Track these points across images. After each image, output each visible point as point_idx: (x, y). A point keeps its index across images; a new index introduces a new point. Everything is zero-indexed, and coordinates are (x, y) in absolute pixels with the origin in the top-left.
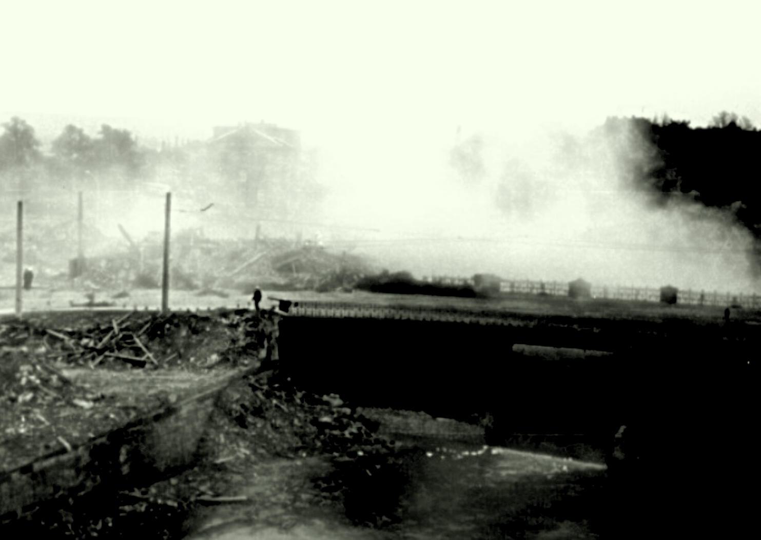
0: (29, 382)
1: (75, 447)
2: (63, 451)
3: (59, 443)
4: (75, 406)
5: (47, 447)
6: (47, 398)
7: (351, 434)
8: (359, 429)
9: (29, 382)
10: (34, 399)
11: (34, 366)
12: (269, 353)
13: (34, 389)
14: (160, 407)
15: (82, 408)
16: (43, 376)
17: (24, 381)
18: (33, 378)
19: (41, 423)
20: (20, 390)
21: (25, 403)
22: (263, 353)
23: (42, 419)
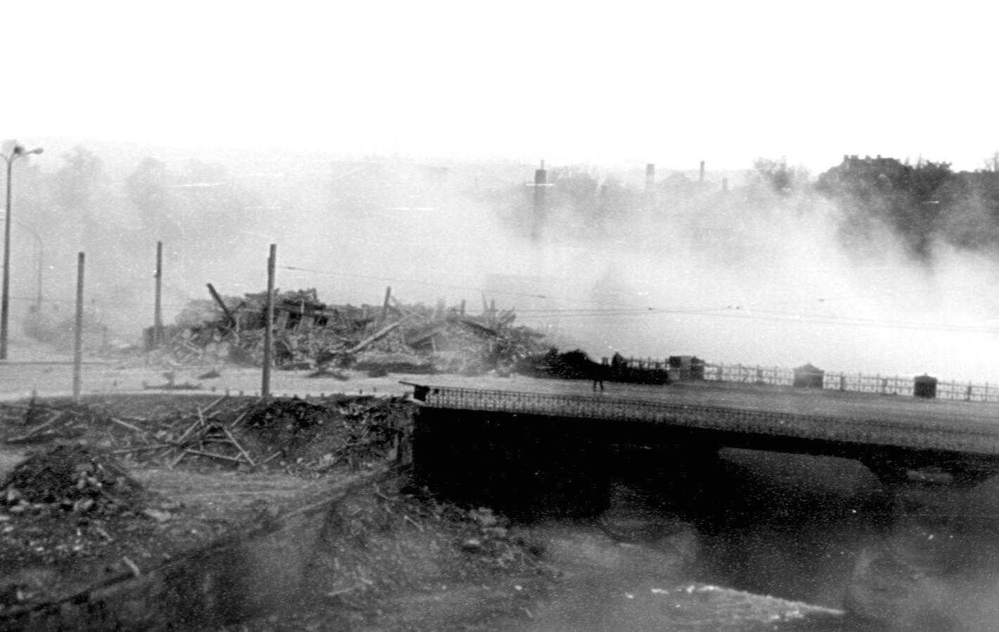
0: (88, 485)
1: (145, 571)
2: (131, 575)
3: (124, 564)
4: (145, 517)
5: (108, 570)
6: (110, 506)
7: (507, 561)
8: (517, 556)
9: (88, 485)
10: (94, 507)
11: (94, 464)
12: (400, 455)
13: (94, 495)
14: (256, 521)
15: (155, 520)
16: (105, 478)
17: (81, 484)
18: (92, 480)
19: (102, 538)
20: (77, 495)
21: (83, 514)
22: (393, 454)
23: (104, 534)
